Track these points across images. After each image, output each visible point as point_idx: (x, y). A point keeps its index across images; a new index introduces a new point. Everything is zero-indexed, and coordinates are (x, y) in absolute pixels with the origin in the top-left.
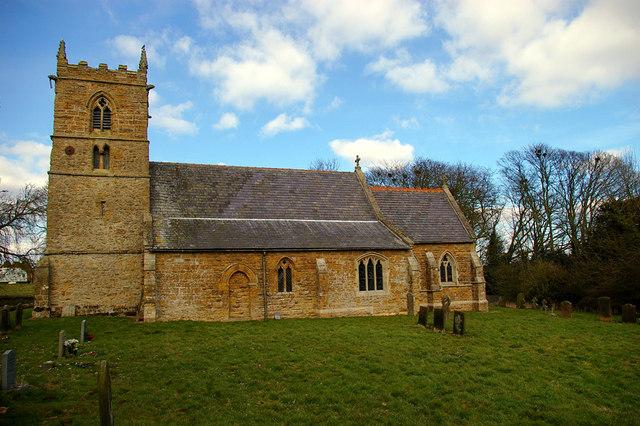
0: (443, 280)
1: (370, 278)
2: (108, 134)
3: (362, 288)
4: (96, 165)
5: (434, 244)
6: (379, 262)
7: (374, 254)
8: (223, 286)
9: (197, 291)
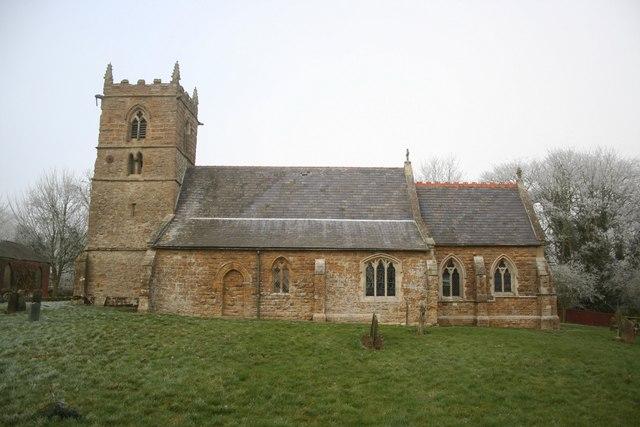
0: (498, 289)
1: (382, 283)
2: (143, 142)
3: (369, 293)
4: (132, 172)
5: (486, 246)
6: (391, 265)
7: (384, 255)
8: (218, 283)
9: (192, 287)
